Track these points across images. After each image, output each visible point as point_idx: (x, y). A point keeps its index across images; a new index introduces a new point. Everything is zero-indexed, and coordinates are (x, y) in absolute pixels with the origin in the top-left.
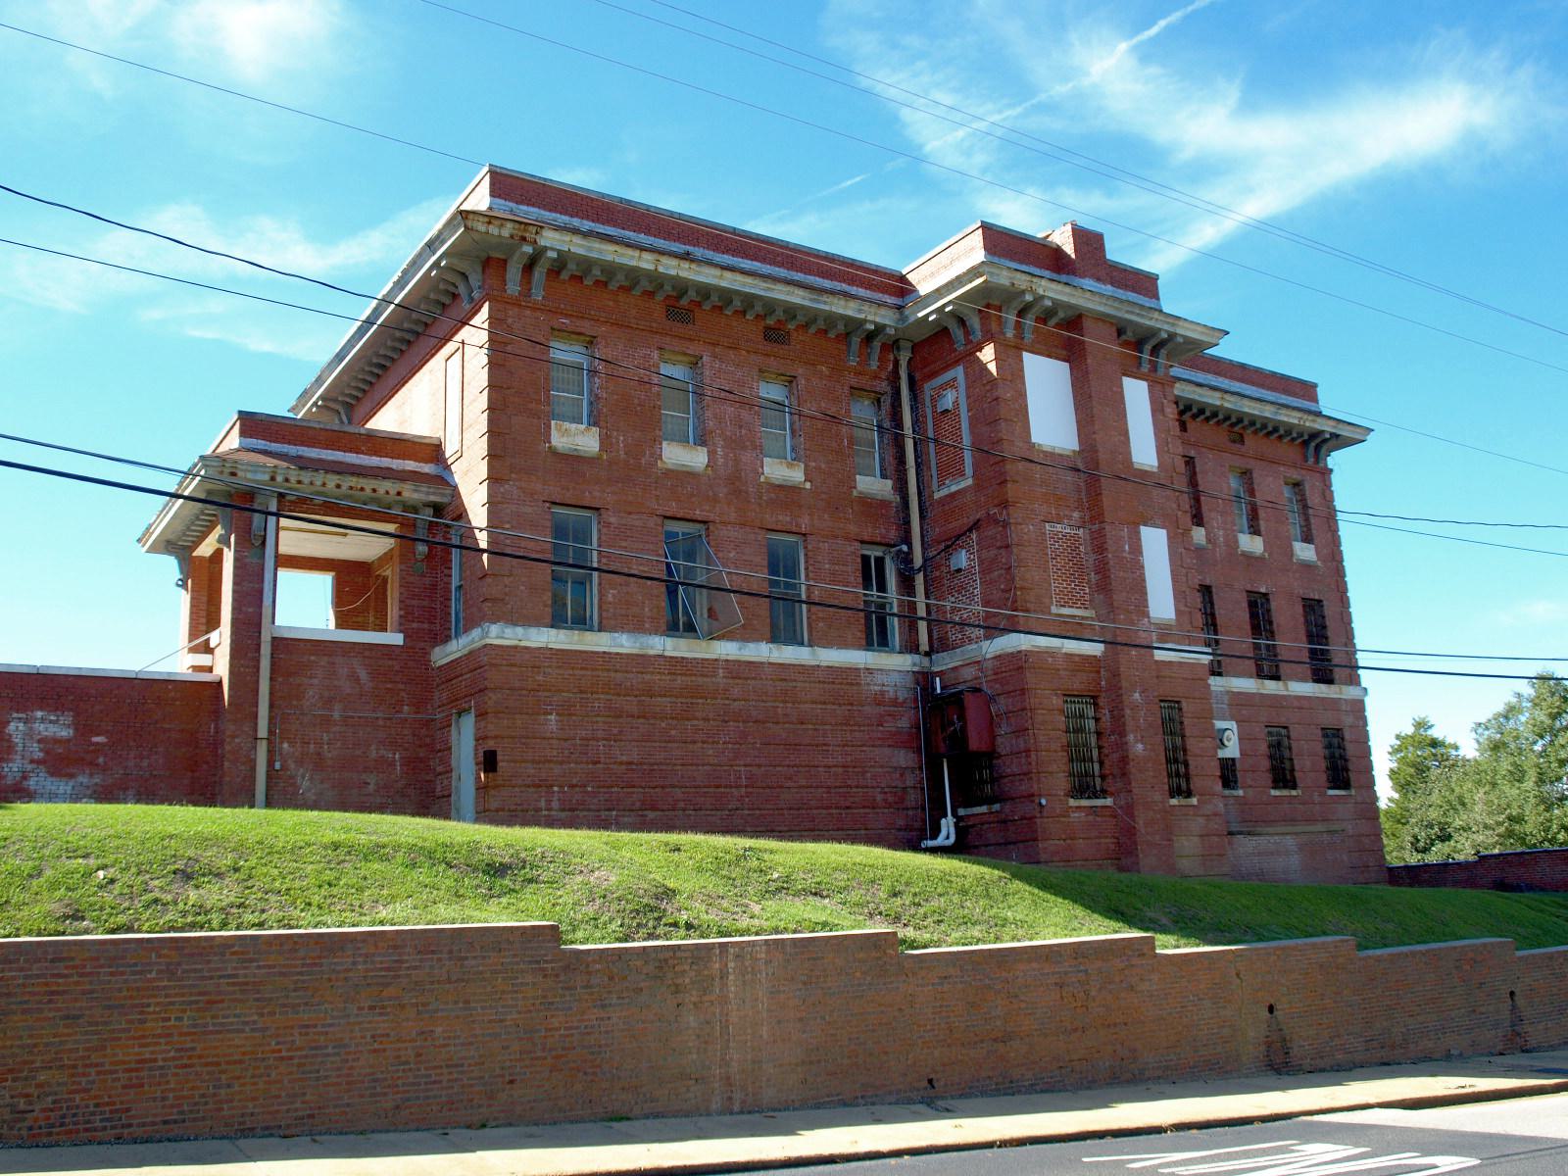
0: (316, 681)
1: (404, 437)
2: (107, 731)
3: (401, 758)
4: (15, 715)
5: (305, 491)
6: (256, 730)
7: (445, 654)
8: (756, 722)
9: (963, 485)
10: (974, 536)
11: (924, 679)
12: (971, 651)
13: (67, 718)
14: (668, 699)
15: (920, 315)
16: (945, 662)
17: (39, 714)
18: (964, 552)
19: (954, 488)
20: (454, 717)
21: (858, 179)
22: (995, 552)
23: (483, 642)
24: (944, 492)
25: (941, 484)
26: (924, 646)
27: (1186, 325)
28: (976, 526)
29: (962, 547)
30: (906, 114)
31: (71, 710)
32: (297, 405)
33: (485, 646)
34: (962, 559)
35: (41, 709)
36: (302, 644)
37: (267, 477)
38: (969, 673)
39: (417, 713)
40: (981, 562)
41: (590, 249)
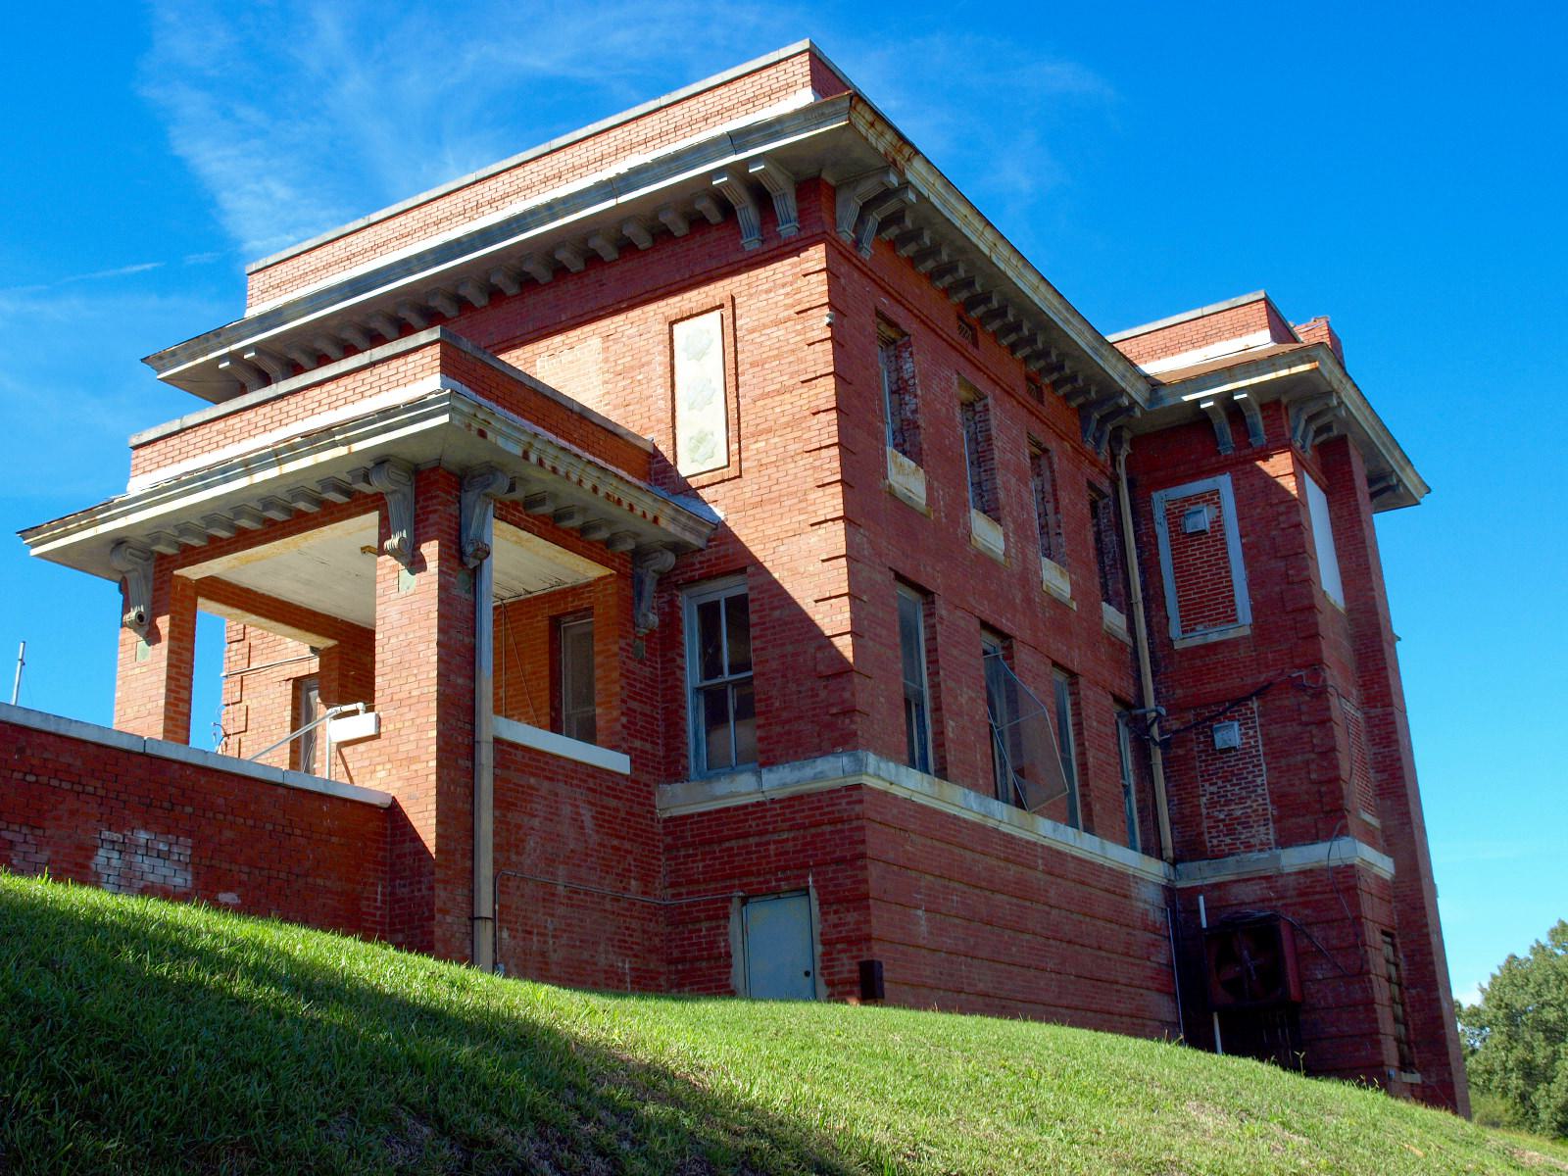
0: (536, 822)
1: (618, 431)
2: (241, 883)
3: (632, 969)
4: (106, 834)
5: (540, 481)
6: (471, 900)
7: (678, 800)
8: (1069, 942)
9: (1232, 633)
10: (1255, 704)
11: (1177, 900)
12: (1257, 861)
13: (183, 850)
14: (1005, 897)
15: (1186, 398)
16: (1201, 874)
17: (143, 836)
18: (1236, 724)
19: (1214, 637)
20: (736, 902)
21: (148, 266)
22: (1299, 729)
23: (852, 781)
24: (1196, 640)
25: (1187, 629)
26: (1169, 853)
27: (1412, 475)
28: (1261, 692)
29: (1232, 719)
30: (227, 199)
31: (189, 834)
32: (173, 354)
33: (858, 787)
34: (1230, 735)
35: (146, 829)
36: (520, 753)
37: (518, 451)
38: (1248, 893)
39: (644, 893)
40: (1268, 741)
41: (945, 202)
